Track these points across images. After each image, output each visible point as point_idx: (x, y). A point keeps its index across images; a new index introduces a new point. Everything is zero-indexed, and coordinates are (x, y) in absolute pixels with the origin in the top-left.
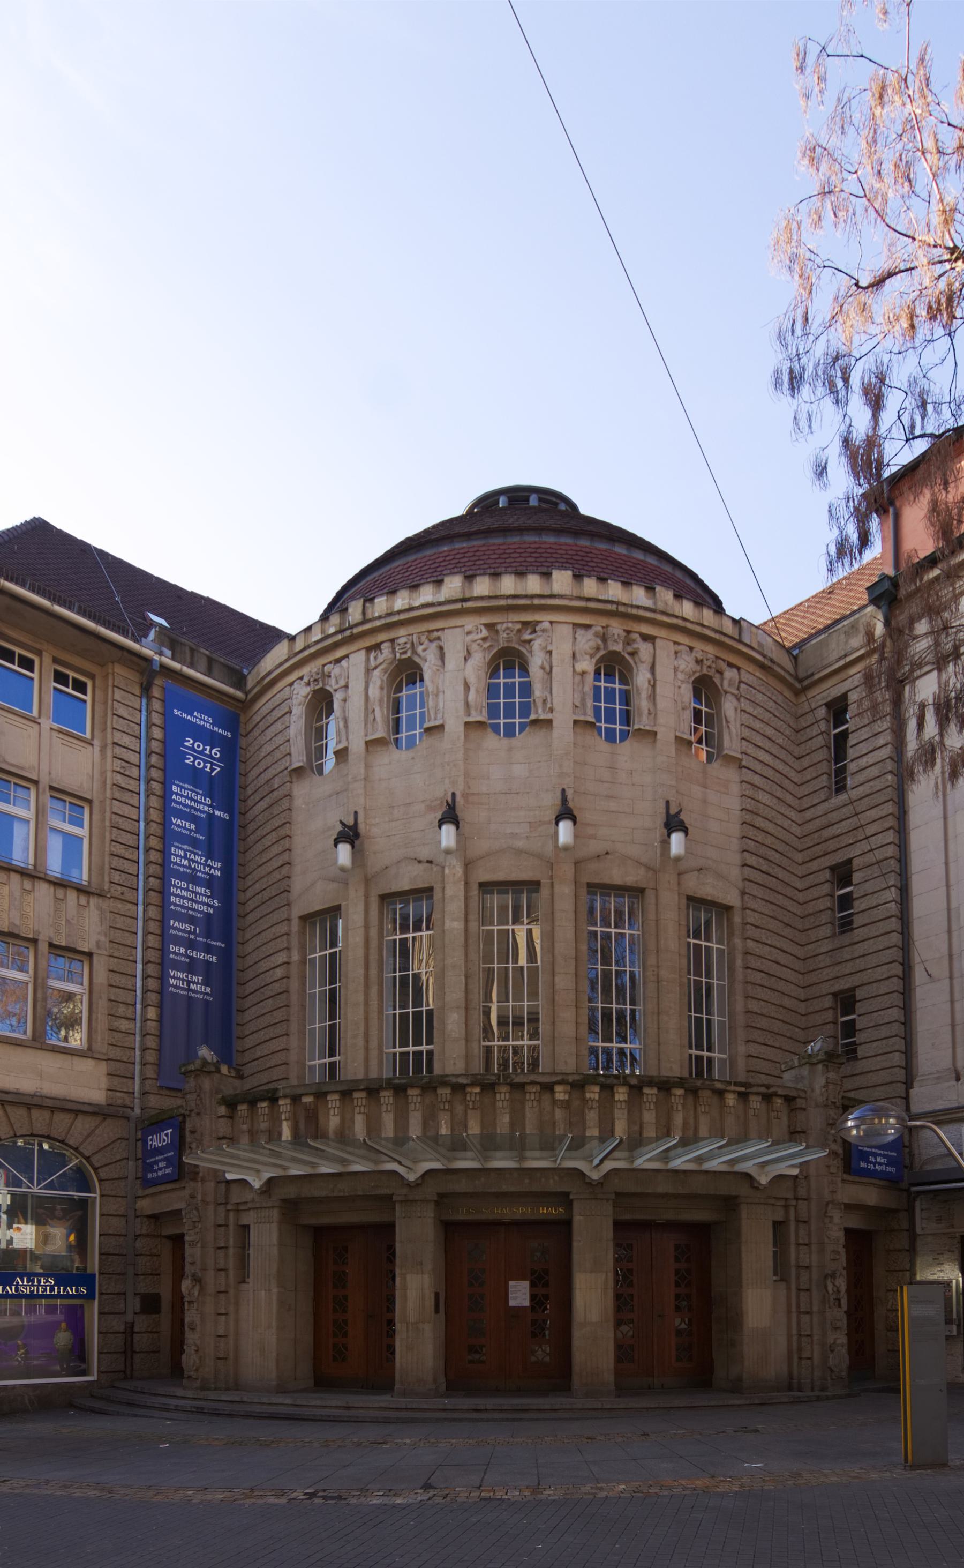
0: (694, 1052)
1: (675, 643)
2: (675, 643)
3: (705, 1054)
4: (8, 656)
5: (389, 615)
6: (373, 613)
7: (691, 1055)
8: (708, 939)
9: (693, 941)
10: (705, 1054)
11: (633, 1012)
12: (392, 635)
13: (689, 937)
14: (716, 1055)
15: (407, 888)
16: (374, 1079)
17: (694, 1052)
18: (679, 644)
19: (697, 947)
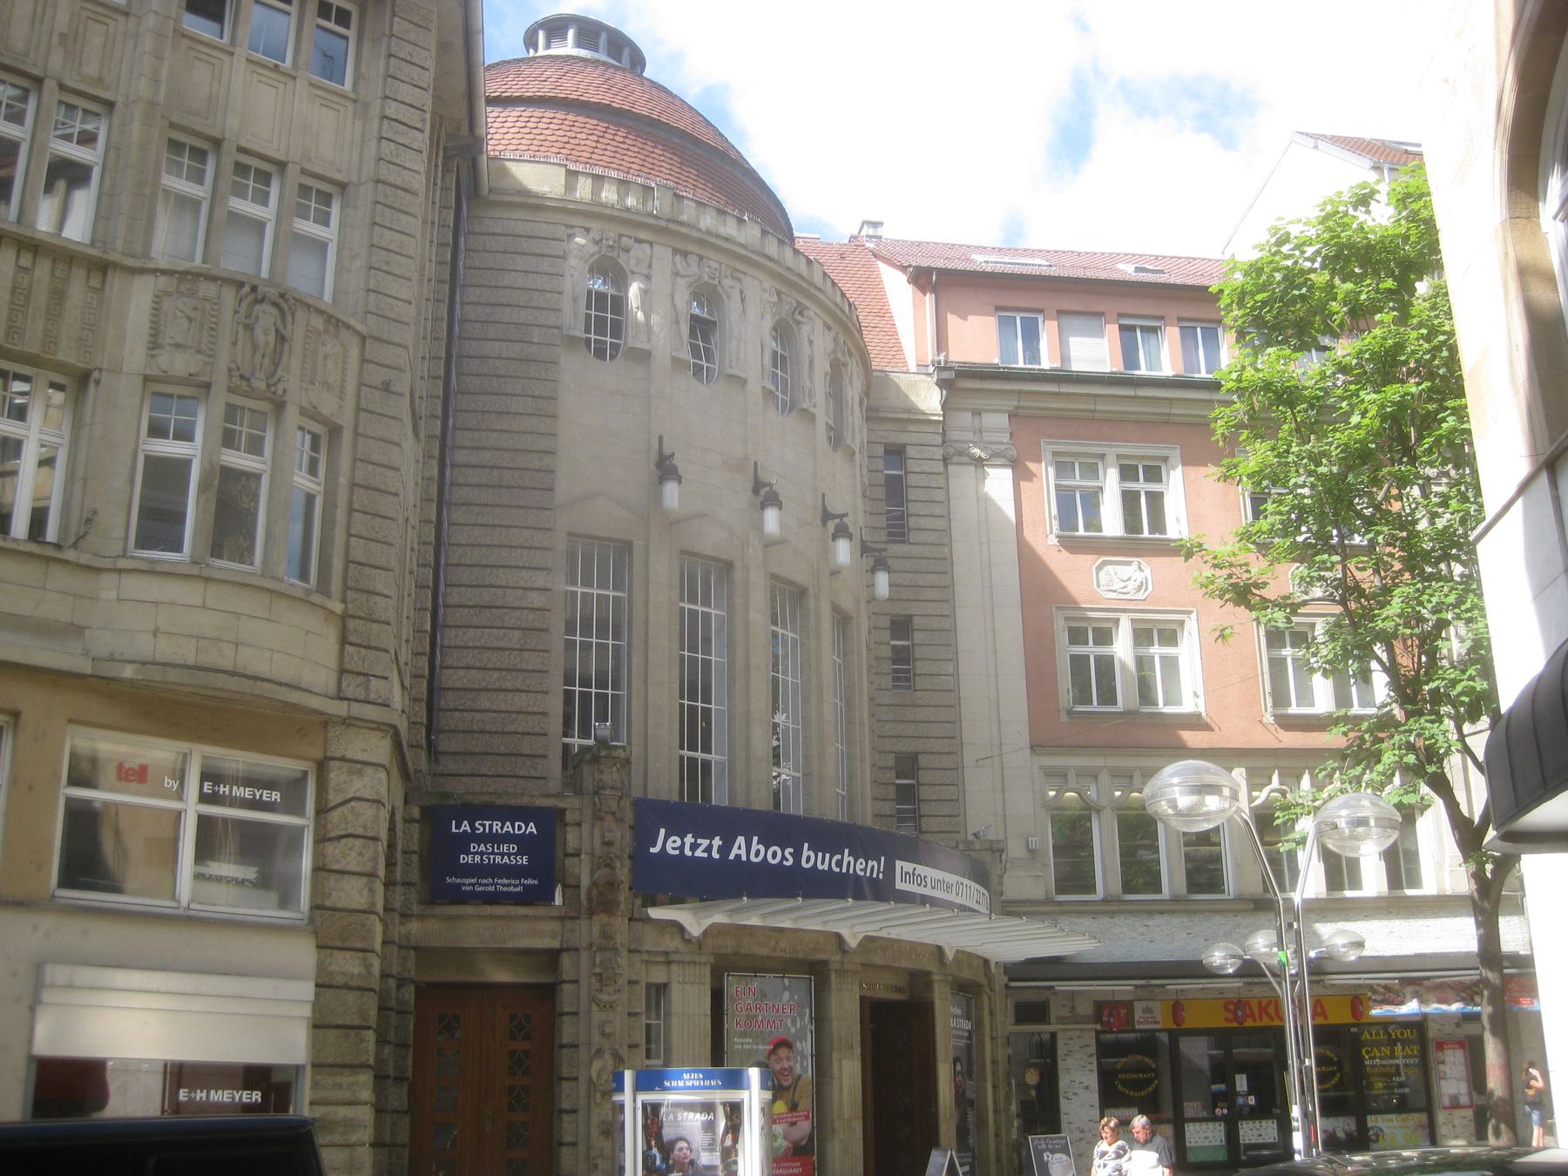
0: (686, 753)
1: (567, 226)
2: (567, 226)
3: (699, 755)
4: (3, 82)
5: (709, 233)
6: (1154, 362)
7: (682, 758)
8: (706, 603)
9: (687, 606)
10: (699, 755)
11: (682, 697)
12: (702, 252)
13: (682, 599)
14: (713, 757)
15: (710, 553)
16: (759, 812)
17: (686, 753)
18: (572, 227)
19: (693, 613)
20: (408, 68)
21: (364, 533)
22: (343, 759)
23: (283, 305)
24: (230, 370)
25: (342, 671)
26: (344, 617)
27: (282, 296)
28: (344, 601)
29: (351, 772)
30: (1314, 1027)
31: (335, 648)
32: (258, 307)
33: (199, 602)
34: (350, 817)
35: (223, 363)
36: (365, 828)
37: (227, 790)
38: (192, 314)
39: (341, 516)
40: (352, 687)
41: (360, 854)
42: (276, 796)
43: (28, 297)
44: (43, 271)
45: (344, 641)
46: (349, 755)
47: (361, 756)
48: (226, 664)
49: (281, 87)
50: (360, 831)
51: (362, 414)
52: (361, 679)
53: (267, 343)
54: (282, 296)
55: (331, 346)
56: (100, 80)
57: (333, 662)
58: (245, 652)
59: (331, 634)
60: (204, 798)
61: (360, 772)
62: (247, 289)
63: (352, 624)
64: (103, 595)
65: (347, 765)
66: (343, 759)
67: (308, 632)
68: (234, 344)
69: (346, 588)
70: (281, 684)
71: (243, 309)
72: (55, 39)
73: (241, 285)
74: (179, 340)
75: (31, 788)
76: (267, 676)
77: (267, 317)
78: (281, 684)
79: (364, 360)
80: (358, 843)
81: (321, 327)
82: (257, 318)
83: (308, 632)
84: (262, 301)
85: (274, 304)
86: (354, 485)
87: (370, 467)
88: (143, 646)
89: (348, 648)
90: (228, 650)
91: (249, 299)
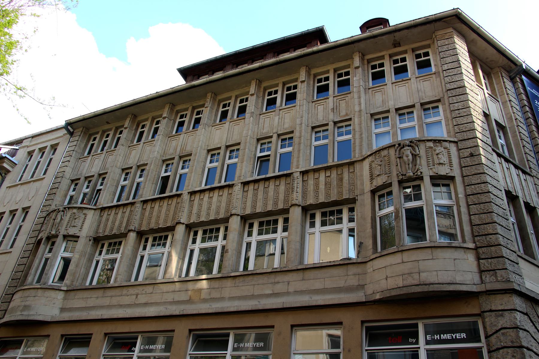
20: (447, 53)
21: (477, 212)
22: (491, 311)
23: (412, 144)
24: (397, 174)
25: (481, 272)
26: (476, 249)
27: (411, 142)
28: (474, 242)
29: (497, 316)
30: (368, 347)
31: (475, 263)
32: (402, 150)
33: (400, 261)
34: (502, 338)
35: (395, 173)
36: (512, 342)
37: (438, 337)
38: (381, 163)
39: (464, 209)
40: (487, 278)
41: (513, 356)
42: (463, 335)
43: (330, 184)
44: (334, 174)
45: (478, 258)
46: (493, 308)
47: (500, 308)
48: (416, 282)
49: (407, 84)
50: (510, 344)
51: (463, 169)
52: (491, 273)
53: (408, 160)
54: (411, 142)
55: (439, 149)
56: (347, 115)
57: (475, 268)
58: (423, 275)
59: (471, 258)
60: (428, 343)
61: (502, 315)
62: (397, 146)
63: (480, 251)
64: (369, 271)
65: (493, 313)
66: (491, 311)
67: (455, 260)
68: (397, 165)
69: (474, 236)
70: (443, 284)
71: (397, 152)
72: (330, 111)
73: (395, 145)
74: (378, 173)
75: (349, 351)
76: (437, 282)
77: (407, 151)
78: (443, 284)
79: (459, 150)
80: (510, 350)
81: (432, 146)
82: (403, 153)
83: (455, 260)
84: (403, 147)
85: (408, 146)
86: (467, 196)
87: (473, 186)
88: (384, 285)
89: (481, 261)
90: (416, 276)
91: (399, 148)
